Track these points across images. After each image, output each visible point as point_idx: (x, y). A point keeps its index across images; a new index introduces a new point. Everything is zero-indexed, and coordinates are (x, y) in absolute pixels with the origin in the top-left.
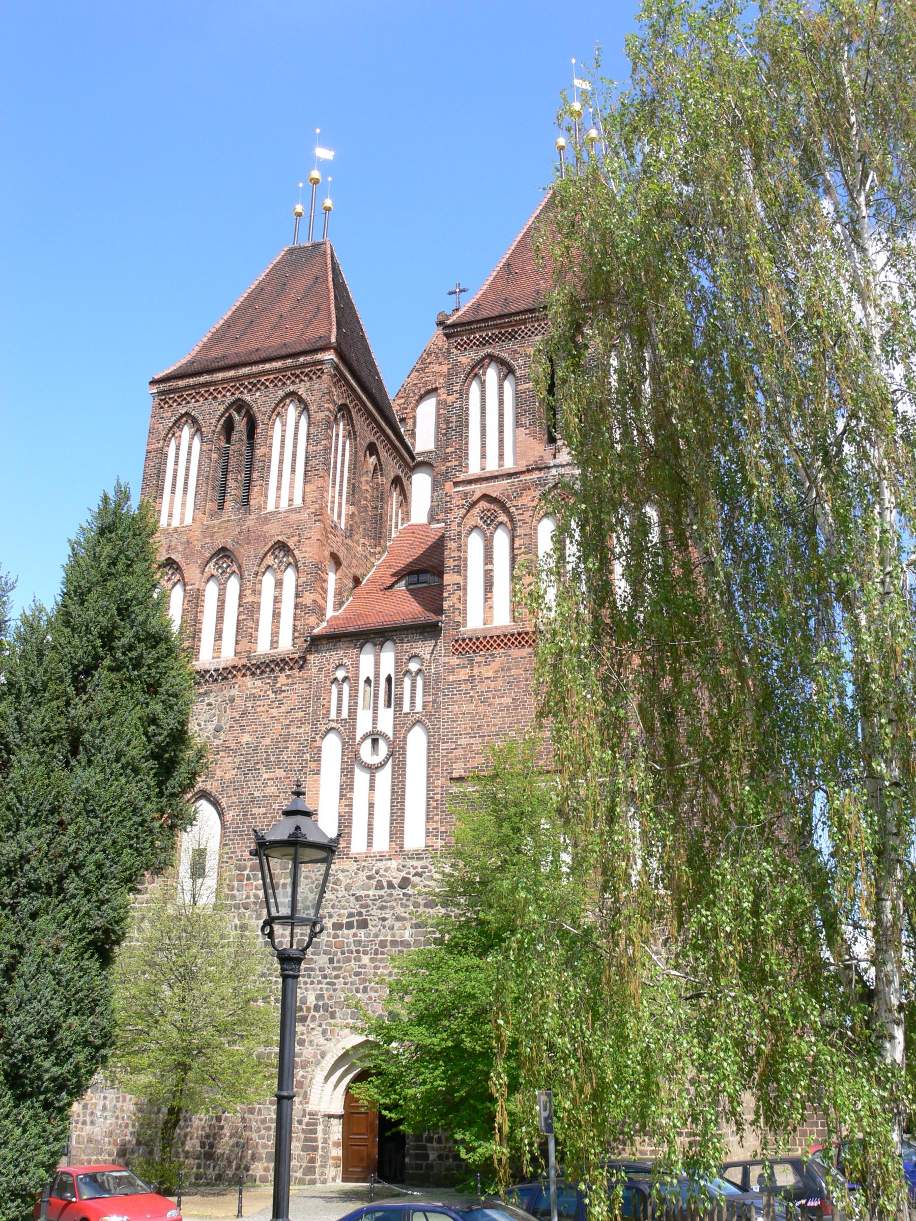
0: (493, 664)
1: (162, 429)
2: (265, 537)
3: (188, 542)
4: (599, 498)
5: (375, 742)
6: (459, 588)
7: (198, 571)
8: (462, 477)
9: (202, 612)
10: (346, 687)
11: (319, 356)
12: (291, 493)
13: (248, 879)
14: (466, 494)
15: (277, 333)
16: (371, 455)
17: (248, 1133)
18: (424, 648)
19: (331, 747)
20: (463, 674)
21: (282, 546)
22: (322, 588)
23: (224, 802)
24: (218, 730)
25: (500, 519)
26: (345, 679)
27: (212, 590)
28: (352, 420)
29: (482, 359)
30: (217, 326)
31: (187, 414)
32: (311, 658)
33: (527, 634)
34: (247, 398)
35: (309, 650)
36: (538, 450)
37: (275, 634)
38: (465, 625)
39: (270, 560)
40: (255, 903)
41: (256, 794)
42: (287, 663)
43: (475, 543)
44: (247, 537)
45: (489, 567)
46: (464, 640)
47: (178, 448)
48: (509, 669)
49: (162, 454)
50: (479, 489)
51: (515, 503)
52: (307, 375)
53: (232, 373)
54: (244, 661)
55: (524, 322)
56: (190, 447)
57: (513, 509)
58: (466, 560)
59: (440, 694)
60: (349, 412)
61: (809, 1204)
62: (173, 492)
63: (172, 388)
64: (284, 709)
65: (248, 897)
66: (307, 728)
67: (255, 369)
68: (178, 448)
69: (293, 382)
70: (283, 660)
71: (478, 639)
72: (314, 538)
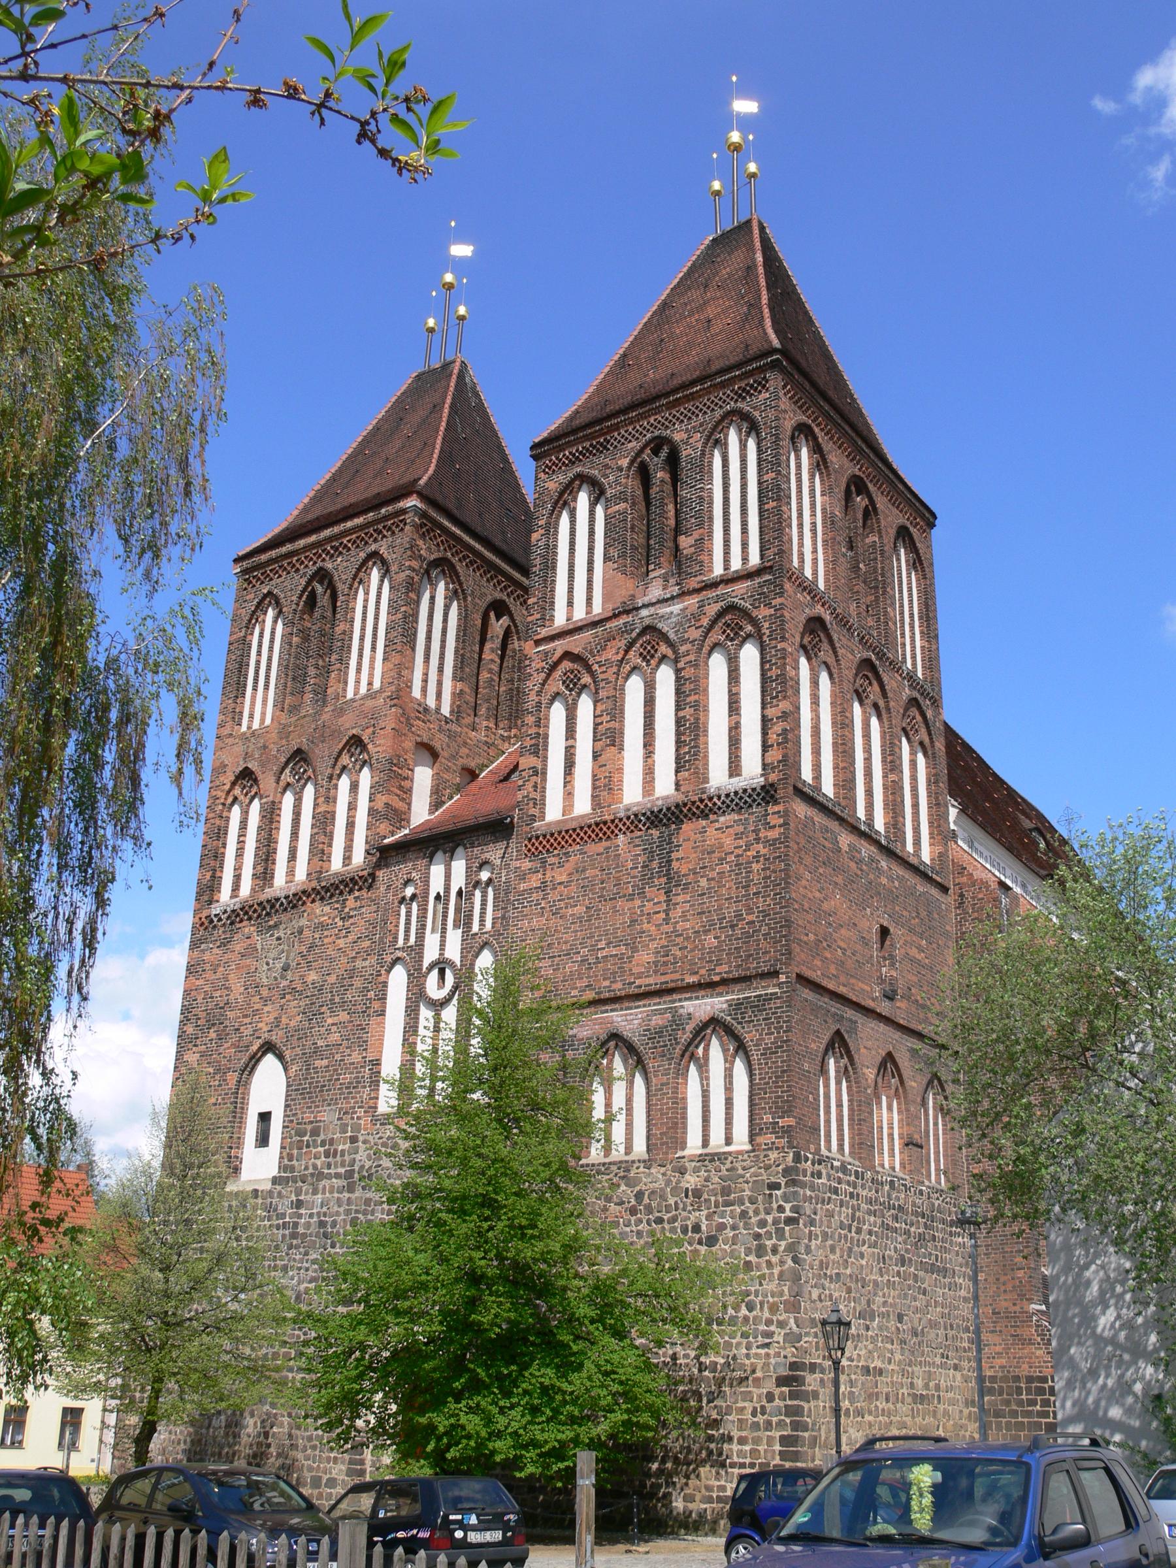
0: (567, 865)
1: (245, 614)
2: (340, 732)
3: (265, 747)
4: (604, 648)
5: (442, 973)
6: (536, 773)
7: (273, 779)
8: (544, 632)
9: (278, 829)
10: (415, 906)
11: (402, 504)
12: (371, 675)
13: (308, 1146)
14: (546, 653)
15: (378, 481)
16: (498, 618)
17: (294, 1453)
18: (494, 853)
19: (398, 979)
20: (534, 881)
21: (356, 743)
22: (401, 787)
23: (288, 1055)
24: (285, 968)
25: (583, 681)
26: (414, 897)
27: (288, 799)
28: (458, 577)
29: (572, 482)
30: (323, 482)
31: (270, 593)
32: (380, 874)
33: (605, 823)
34: (329, 565)
35: (378, 866)
36: (626, 587)
37: (349, 848)
38: (543, 818)
39: (345, 760)
40: (312, 1175)
41: (320, 1043)
42: (356, 883)
43: (557, 713)
44: (323, 734)
45: (571, 742)
46: (537, 838)
47: (261, 635)
48: (584, 870)
49: (245, 644)
50: (560, 646)
51: (598, 658)
52: (389, 529)
53: (313, 538)
54: (314, 884)
55: (616, 427)
56: (273, 633)
57: (596, 667)
58: (546, 736)
59: (510, 907)
60: (452, 567)
61: (421, 1535)
62: (255, 689)
63: (255, 565)
64: (351, 938)
65: (306, 1168)
66: (373, 960)
67: (336, 529)
68: (261, 635)
69: (375, 540)
70: (352, 879)
71: (552, 835)
72: (389, 728)
